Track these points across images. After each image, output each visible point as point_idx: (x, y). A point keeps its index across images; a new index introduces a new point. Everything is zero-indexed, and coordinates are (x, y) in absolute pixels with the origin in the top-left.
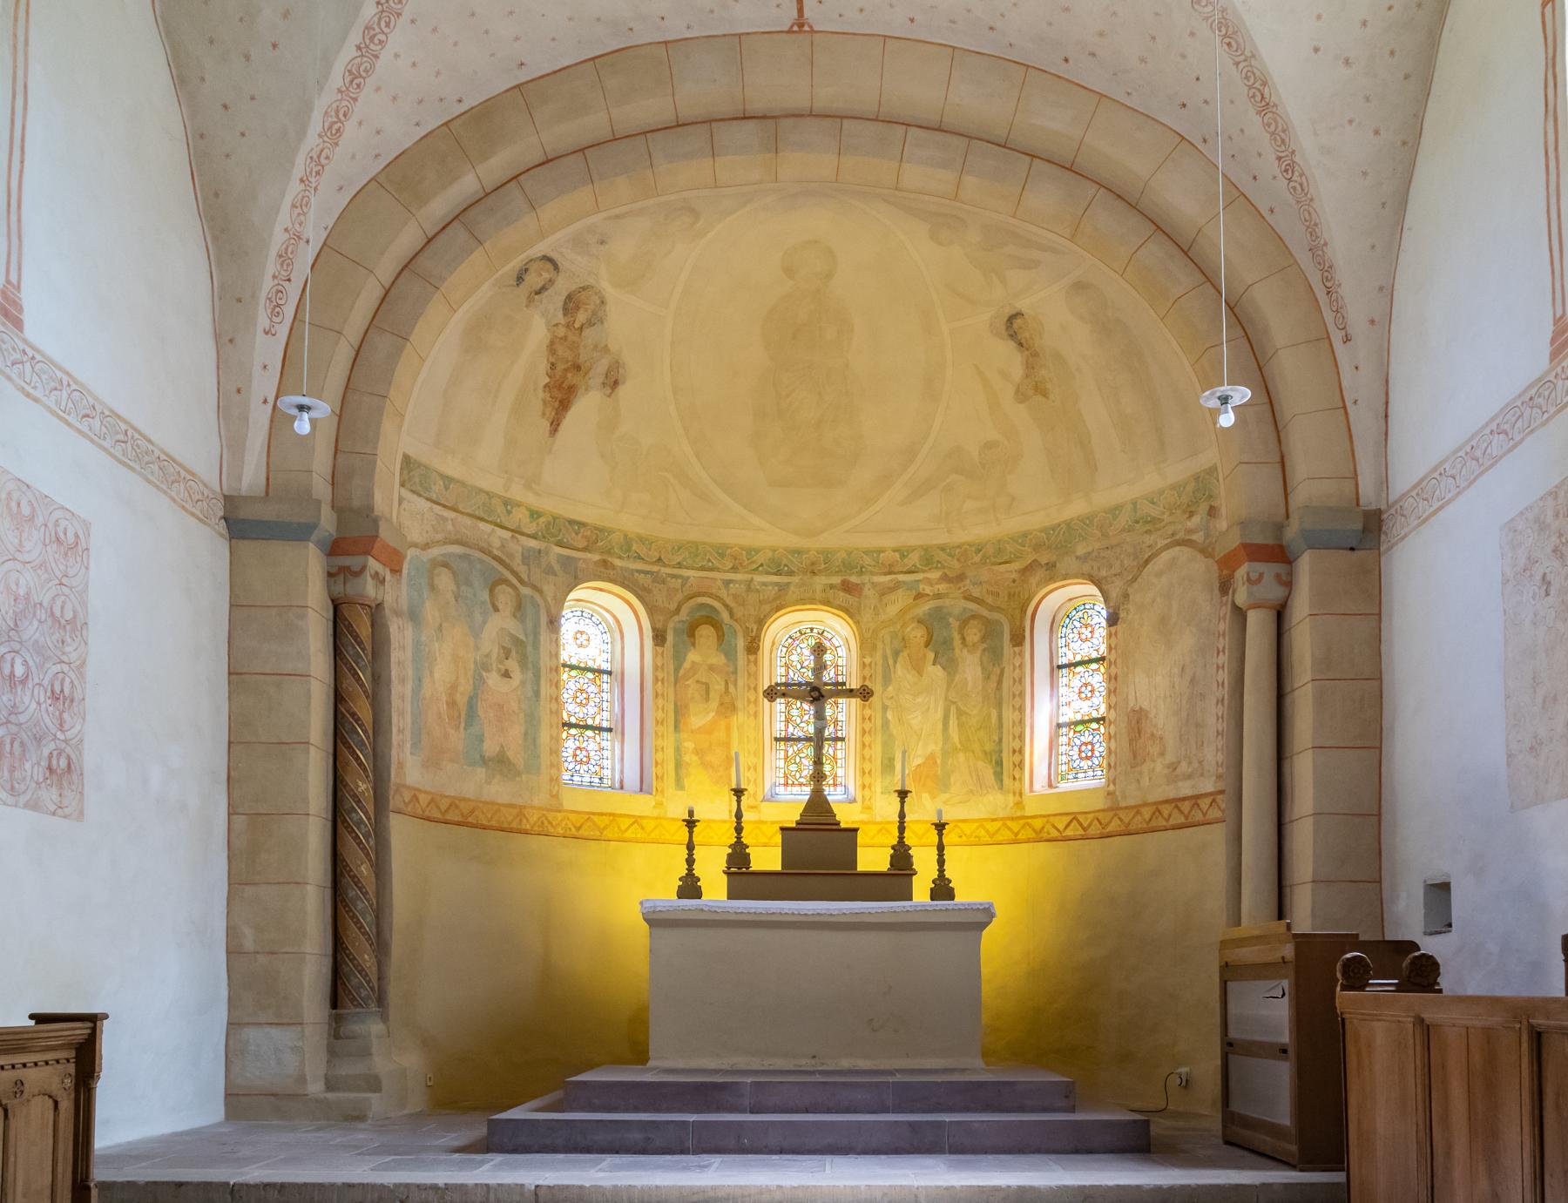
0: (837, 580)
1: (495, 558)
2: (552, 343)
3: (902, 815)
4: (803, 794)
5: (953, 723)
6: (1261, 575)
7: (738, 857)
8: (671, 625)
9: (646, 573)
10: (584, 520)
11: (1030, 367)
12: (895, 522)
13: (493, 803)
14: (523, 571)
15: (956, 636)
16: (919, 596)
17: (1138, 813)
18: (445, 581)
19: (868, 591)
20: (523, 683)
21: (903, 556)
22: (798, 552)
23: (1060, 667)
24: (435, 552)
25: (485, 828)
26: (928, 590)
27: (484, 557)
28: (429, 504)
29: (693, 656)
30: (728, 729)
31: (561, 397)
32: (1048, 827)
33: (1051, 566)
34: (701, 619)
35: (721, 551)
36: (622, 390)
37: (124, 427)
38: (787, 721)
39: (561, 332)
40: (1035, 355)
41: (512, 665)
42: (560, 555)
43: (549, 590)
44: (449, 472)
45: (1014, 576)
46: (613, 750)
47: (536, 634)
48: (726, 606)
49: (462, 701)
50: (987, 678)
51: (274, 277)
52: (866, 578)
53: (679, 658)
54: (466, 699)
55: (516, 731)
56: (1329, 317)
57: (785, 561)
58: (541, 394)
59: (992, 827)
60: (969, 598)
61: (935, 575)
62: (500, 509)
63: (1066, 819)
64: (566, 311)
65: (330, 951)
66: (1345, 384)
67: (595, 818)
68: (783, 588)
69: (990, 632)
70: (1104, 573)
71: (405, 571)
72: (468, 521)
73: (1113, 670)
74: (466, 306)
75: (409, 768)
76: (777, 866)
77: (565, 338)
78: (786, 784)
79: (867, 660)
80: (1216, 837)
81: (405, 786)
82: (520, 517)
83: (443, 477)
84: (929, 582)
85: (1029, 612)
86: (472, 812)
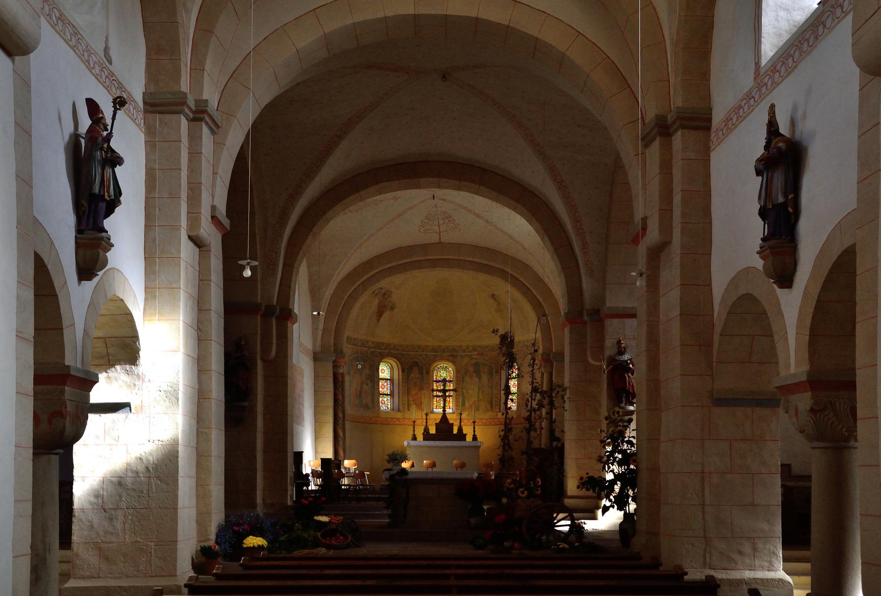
7: (426, 430)
29: (412, 375)
31: (380, 314)
34: (415, 373)
35: (419, 347)
36: (395, 310)
75: (349, 410)
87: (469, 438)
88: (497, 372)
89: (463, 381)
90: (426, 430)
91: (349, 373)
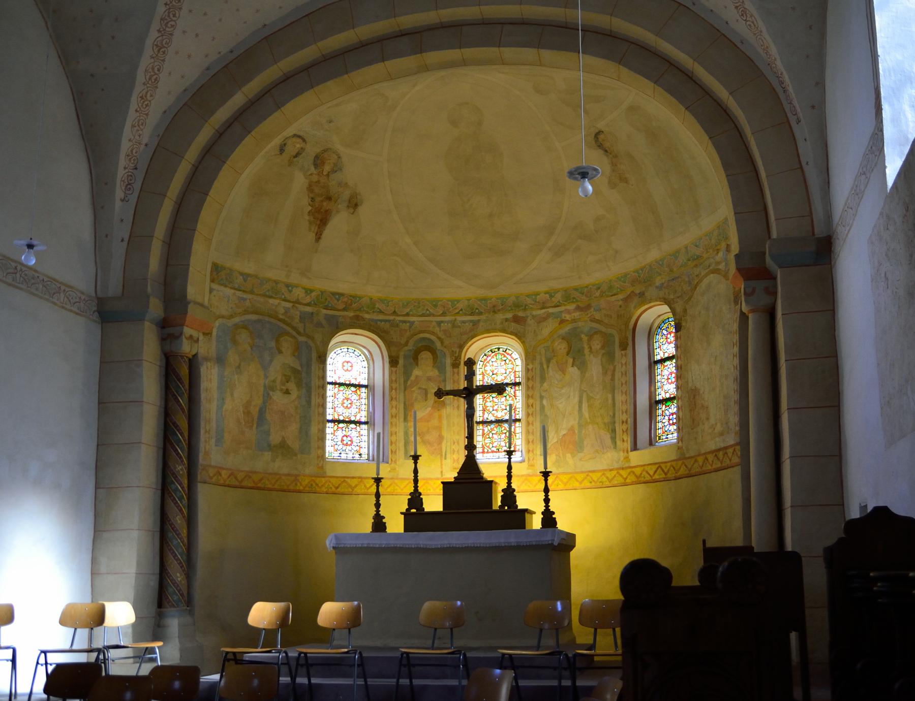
0: (509, 315)
1: (280, 320)
2: (310, 185)
3: (416, 472)
4: (460, 458)
5: (585, 405)
6: (754, 290)
7: (415, 499)
8: (402, 353)
9: (386, 321)
10: (340, 291)
11: (614, 165)
12: (539, 274)
13: (276, 474)
14: (300, 327)
15: (586, 346)
16: (562, 322)
17: (696, 461)
18: (243, 337)
19: (530, 321)
20: (299, 397)
21: (551, 296)
22: (484, 299)
23: (657, 362)
24: (237, 320)
25: (270, 490)
26: (568, 317)
27: (272, 320)
28: (233, 291)
29: (417, 372)
30: (440, 417)
31: (321, 219)
32: (644, 473)
33: (642, 294)
35: (435, 303)
36: (360, 209)
37: (14, 264)
38: (484, 410)
39: (315, 178)
40: (616, 156)
41: (292, 386)
42: (326, 315)
43: (318, 337)
44: (247, 271)
45: (620, 303)
46: (368, 436)
47: (309, 365)
48: (439, 338)
49: (255, 411)
50: (605, 373)
51: (125, 168)
52: (528, 313)
53: (407, 374)
54: (257, 409)
55: (293, 428)
56: (787, 109)
57: (476, 306)
58: (307, 218)
59: (610, 475)
60: (593, 320)
61: (572, 307)
62: (284, 290)
63: (654, 468)
64: (316, 165)
65: (157, 571)
66: (800, 151)
67: (348, 480)
68: (475, 323)
69: (607, 342)
70: (672, 297)
71: (214, 333)
72: (262, 299)
73: (679, 362)
74: (248, 171)
75: (212, 453)
76: (440, 508)
77: (318, 182)
78: (483, 452)
79: (530, 367)
80: (735, 474)
81: (210, 466)
82: (298, 293)
83: (242, 274)
84: (569, 312)
85: (631, 327)
86: (261, 480)
87: (536, 522)
88: (623, 346)
89: (543, 379)
90: (415, 499)
91: (220, 360)
